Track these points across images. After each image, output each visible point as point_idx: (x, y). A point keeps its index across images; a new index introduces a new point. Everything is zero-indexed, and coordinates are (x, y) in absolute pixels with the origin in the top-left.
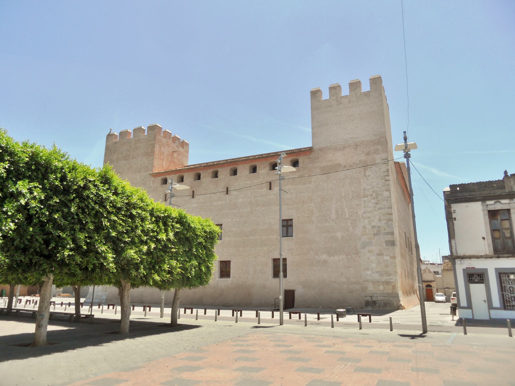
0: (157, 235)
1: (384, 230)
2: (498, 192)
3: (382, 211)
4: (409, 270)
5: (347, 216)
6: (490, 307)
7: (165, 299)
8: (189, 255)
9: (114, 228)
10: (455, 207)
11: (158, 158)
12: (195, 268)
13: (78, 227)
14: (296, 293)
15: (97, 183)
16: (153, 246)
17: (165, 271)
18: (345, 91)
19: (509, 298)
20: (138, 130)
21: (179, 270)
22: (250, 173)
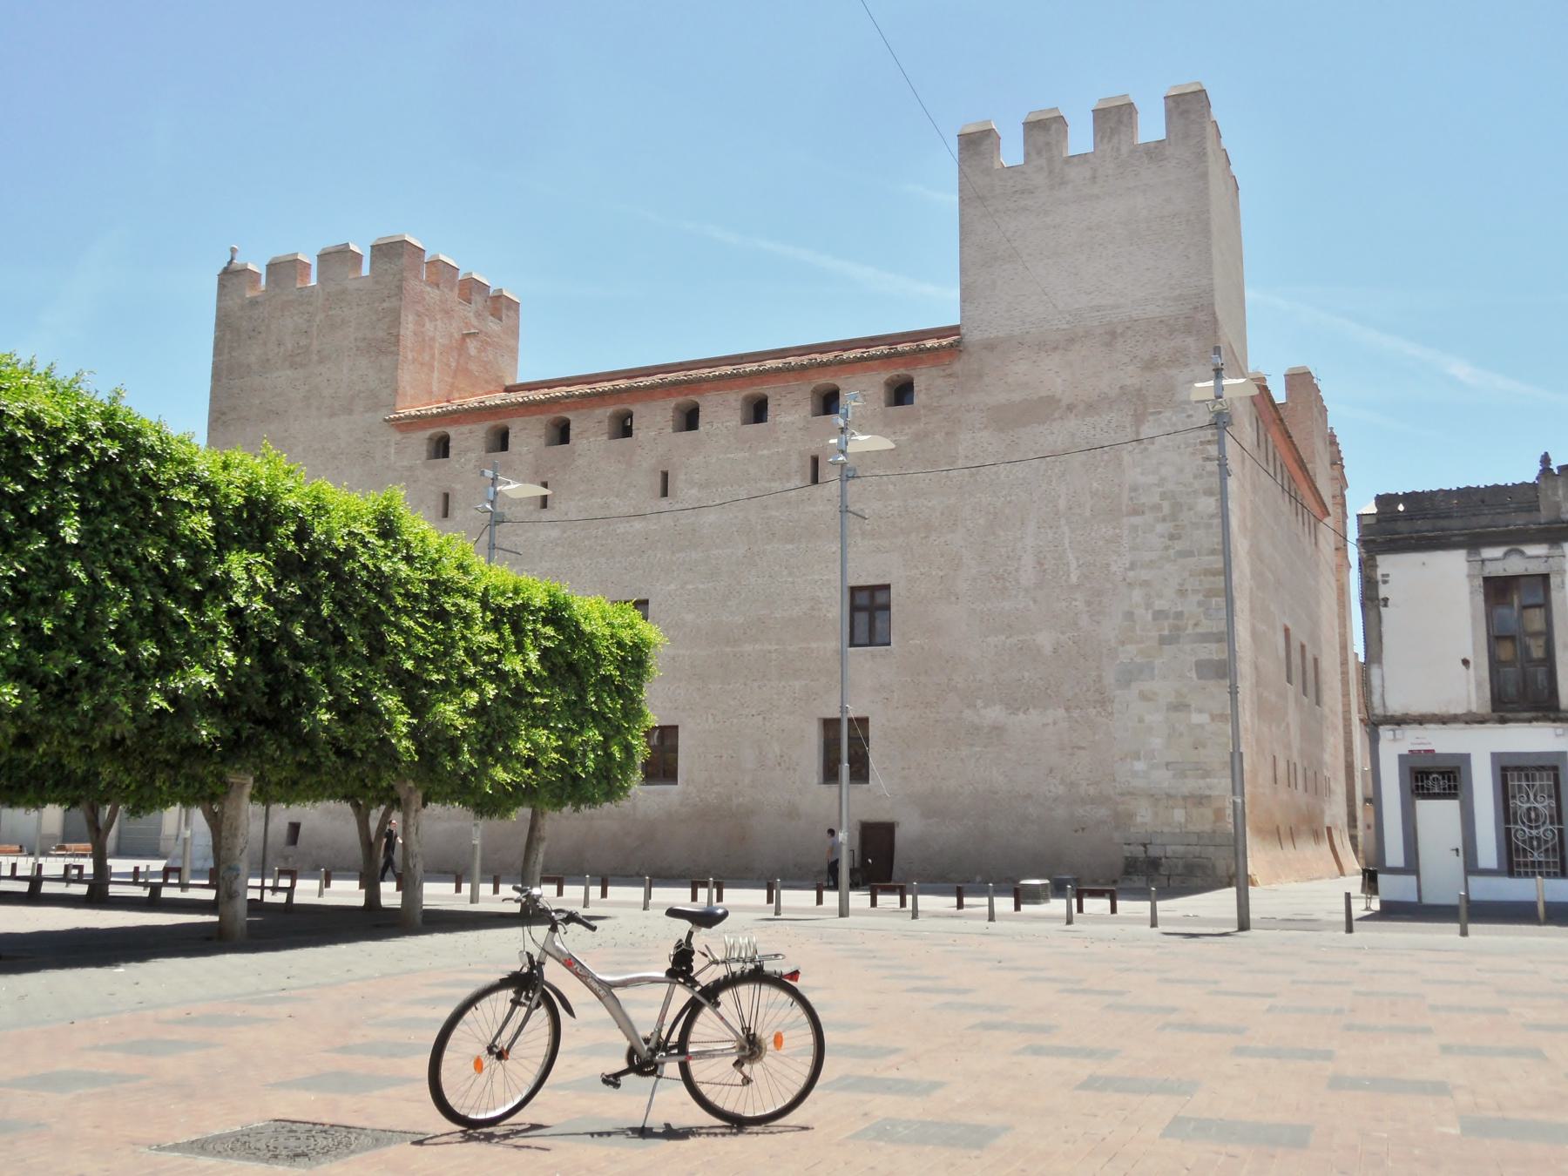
0: (499, 661)
1: (1196, 625)
2: (1519, 521)
3: (1191, 561)
4: (1296, 758)
5: (1074, 579)
6: (1471, 867)
7: (483, 849)
8: (578, 712)
9: (408, 649)
10: (1387, 564)
11: (414, 360)
12: (593, 750)
13: (333, 650)
14: (899, 834)
15: (371, 539)
16: (491, 690)
17: (518, 757)
18: (1080, 139)
19: (1524, 842)
20: (337, 258)
21: (554, 755)
22: (745, 422)
